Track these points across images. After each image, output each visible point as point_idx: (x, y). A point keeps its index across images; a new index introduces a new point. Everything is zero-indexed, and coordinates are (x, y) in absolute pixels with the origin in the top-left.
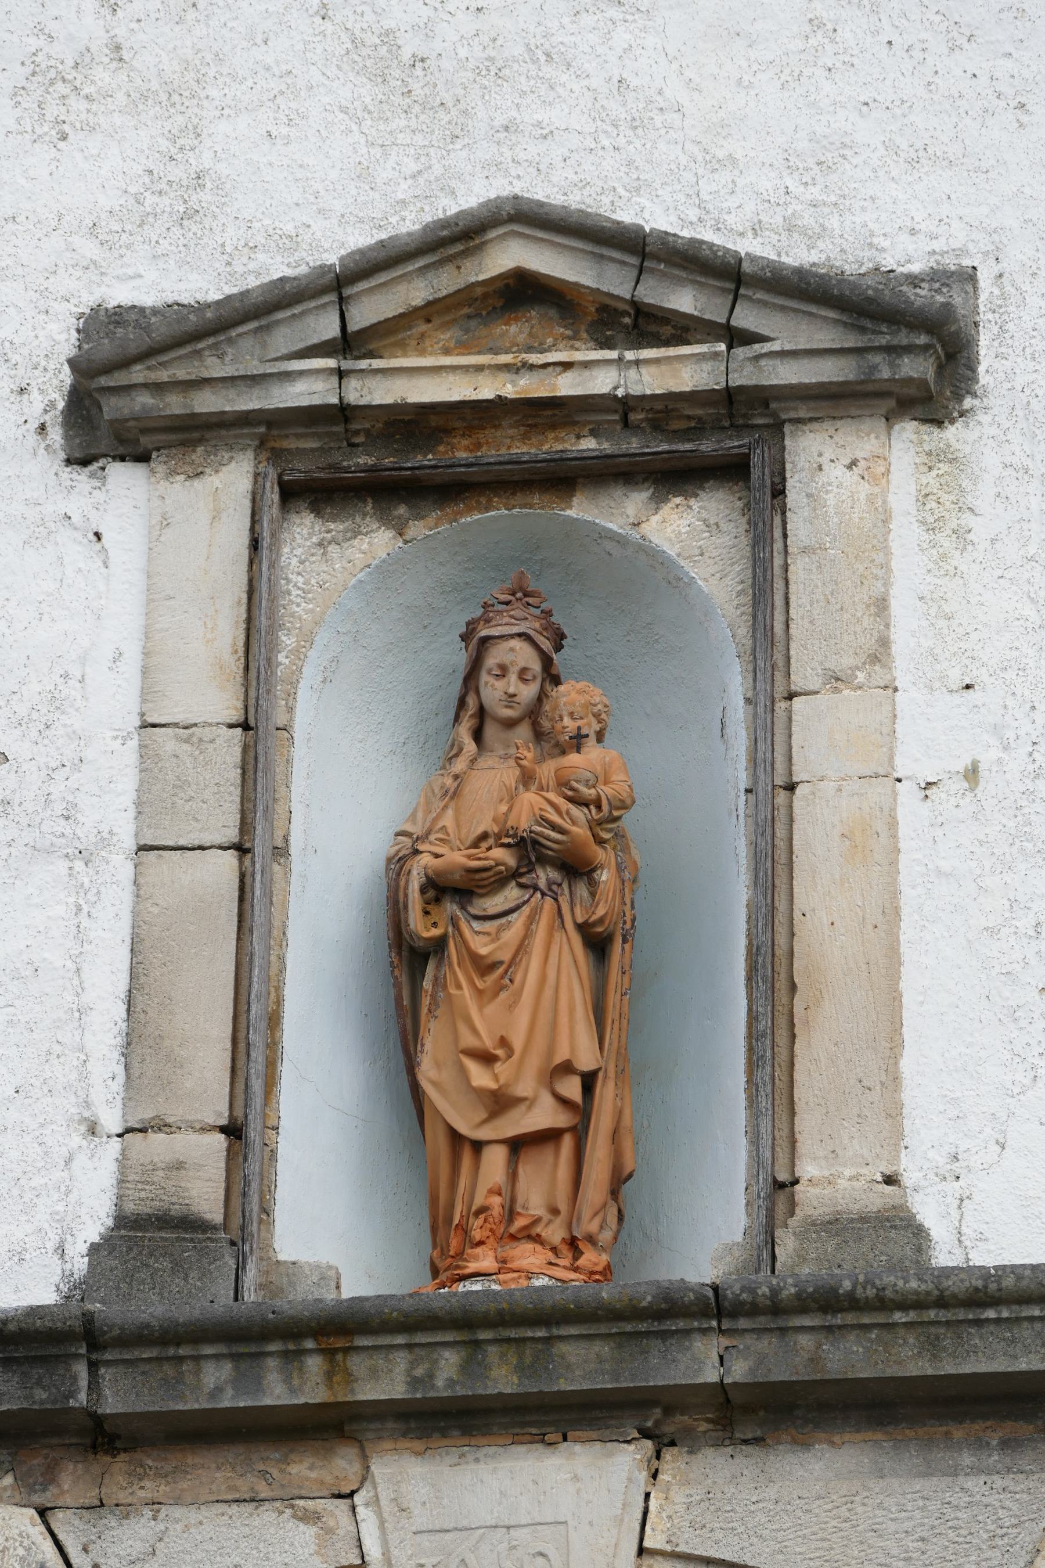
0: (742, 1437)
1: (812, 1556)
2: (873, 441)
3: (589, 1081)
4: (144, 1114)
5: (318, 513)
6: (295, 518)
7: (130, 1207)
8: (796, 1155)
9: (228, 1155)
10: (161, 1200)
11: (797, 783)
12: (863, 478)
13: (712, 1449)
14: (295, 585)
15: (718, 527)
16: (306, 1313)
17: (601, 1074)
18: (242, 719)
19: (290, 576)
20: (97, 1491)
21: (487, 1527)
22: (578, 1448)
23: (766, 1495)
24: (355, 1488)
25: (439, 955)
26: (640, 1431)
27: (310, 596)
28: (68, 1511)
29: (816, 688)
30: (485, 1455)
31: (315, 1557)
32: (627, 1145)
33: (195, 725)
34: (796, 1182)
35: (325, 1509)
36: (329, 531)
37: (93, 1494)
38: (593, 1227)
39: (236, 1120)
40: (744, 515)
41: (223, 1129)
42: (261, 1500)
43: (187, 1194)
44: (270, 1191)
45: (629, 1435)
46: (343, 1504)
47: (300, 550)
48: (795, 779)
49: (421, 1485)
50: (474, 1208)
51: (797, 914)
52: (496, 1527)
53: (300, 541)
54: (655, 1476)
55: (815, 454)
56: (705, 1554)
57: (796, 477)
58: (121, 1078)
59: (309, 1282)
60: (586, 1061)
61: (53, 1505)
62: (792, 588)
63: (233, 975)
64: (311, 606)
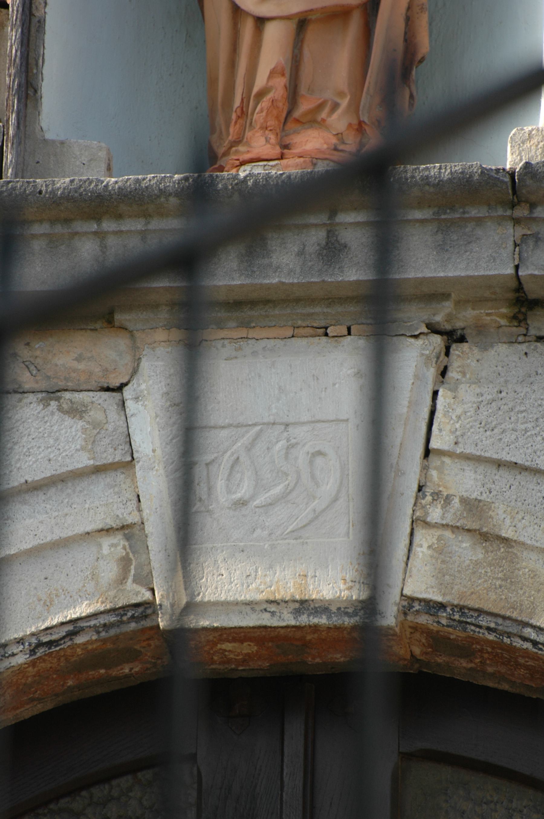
16: (213, 483)
24: (124, 381)
26: (428, 326)
35: (92, 403)
44: (37, 65)
45: (417, 329)
50: (255, 90)
52: (274, 424)
54: (444, 373)
56: (495, 456)
59: (78, 163)
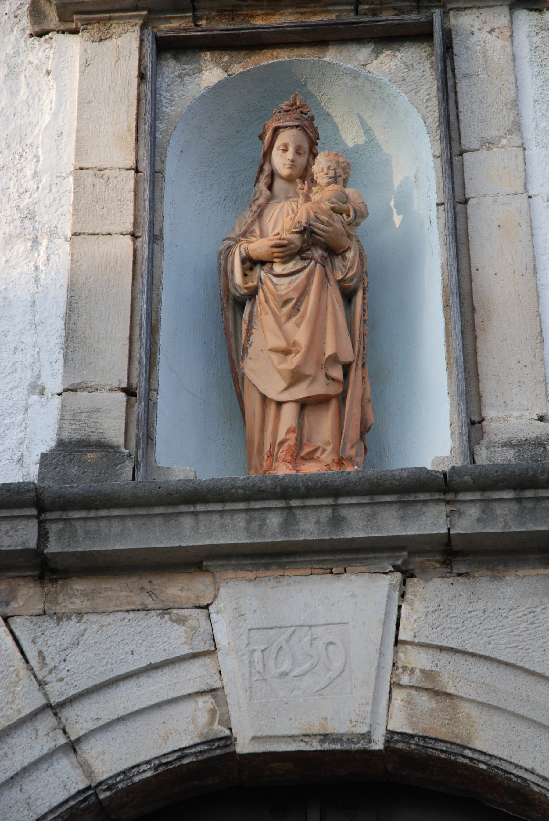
0: (459, 572)
1: (511, 645)
2: (503, 19)
3: (346, 368)
4: (76, 380)
5: (178, 60)
6: (164, 63)
7: (65, 435)
8: (482, 404)
9: (127, 405)
10: (85, 430)
11: (469, 198)
12: (498, 38)
13: (440, 579)
14: (165, 97)
15: (413, 66)
17: (354, 365)
18: (134, 166)
19: (162, 93)
20: (42, 605)
21: (296, 626)
22: (354, 577)
23: (477, 607)
24: (209, 602)
25: (253, 300)
26: (394, 566)
27: (174, 103)
28: (23, 618)
29: (477, 148)
30: (294, 581)
31: (184, 645)
32: (369, 408)
33: (106, 169)
34: (483, 420)
35: (190, 615)
36: (184, 70)
37: (40, 607)
38: (352, 452)
39: (132, 385)
40: (428, 60)
41: (123, 390)
42: (148, 610)
43: (101, 427)
44: (153, 426)
46: (200, 614)
47: (168, 79)
48: (467, 196)
49: (254, 599)
50: (278, 441)
51: (473, 269)
52: (302, 626)
53: (167, 75)
55: (469, 26)
56: (439, 644)
57: (459, 38)
58: (61, 361)
60: (347, 355)
61: (13, 614)
62: (460, 95)
63: (130, 303)
64: (174, 108)
